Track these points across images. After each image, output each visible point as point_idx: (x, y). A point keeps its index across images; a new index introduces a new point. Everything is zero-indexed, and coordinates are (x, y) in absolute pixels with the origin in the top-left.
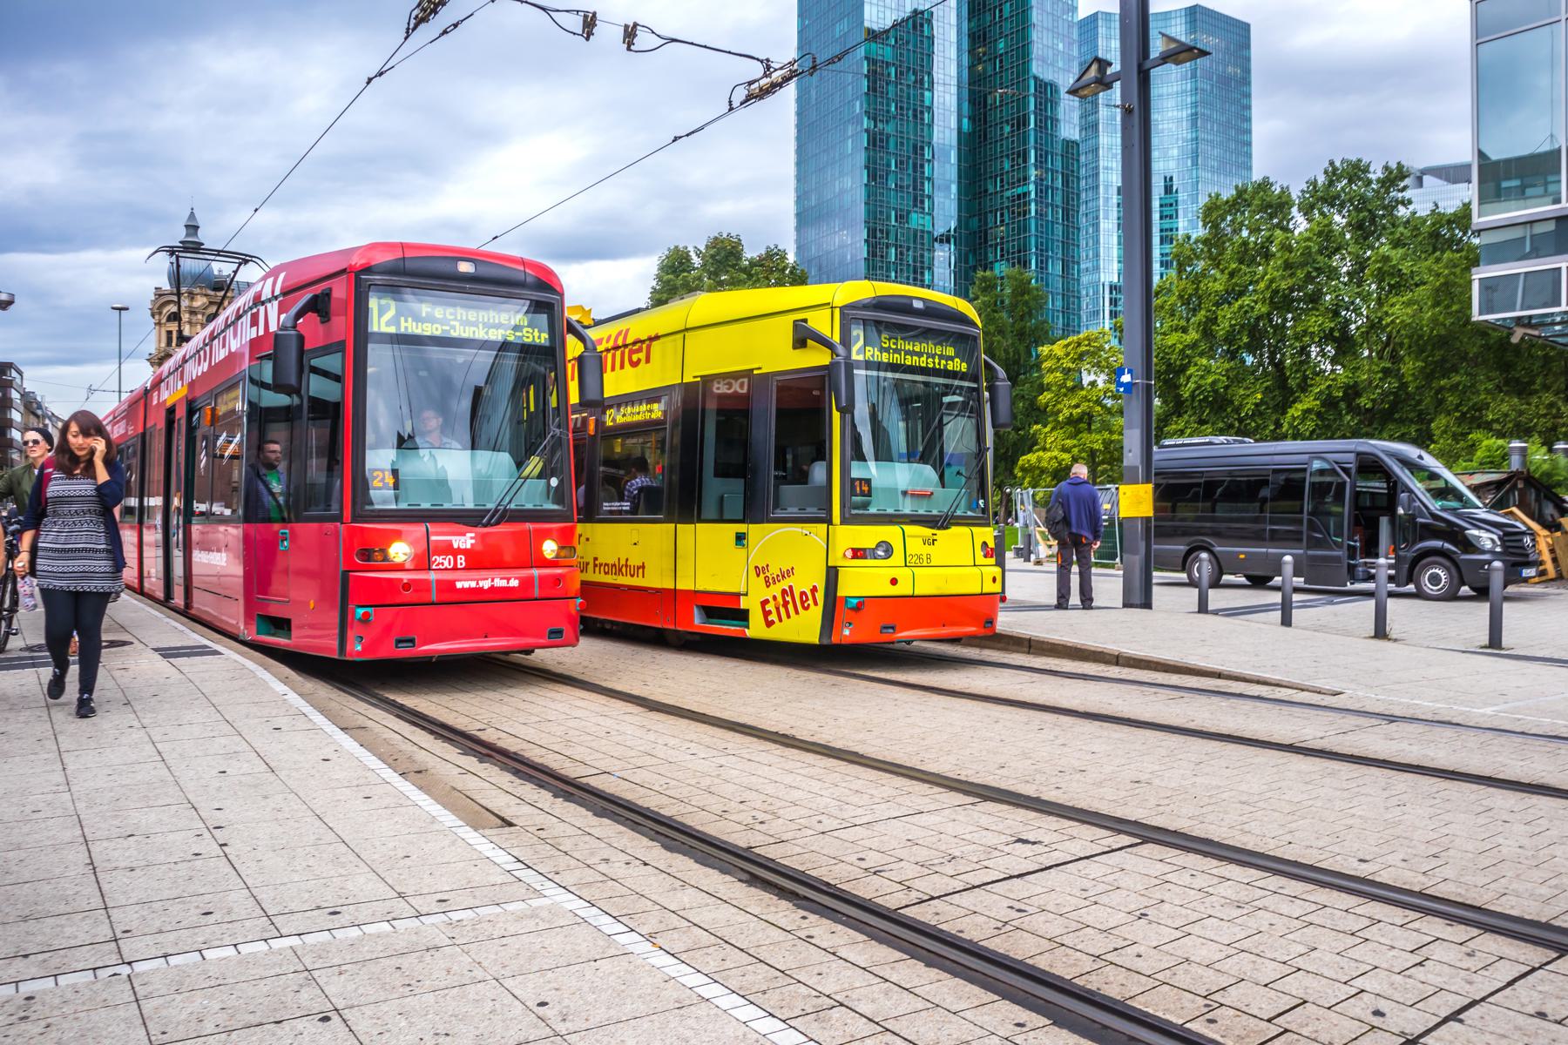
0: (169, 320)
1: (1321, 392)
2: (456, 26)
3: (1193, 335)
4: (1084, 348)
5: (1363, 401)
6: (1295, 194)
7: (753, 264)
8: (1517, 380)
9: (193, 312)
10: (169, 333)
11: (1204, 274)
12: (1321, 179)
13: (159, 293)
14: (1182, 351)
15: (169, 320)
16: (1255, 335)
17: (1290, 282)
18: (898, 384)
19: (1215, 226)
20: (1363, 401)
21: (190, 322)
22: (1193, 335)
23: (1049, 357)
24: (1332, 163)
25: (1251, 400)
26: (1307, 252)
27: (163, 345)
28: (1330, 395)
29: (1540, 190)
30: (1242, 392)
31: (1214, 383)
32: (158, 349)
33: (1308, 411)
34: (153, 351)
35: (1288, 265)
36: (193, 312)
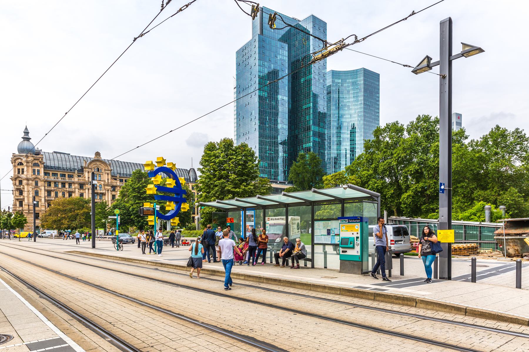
0: (18, 165)
1: (413, 189)
2: (187, 6)
3: (371, 172)
4: (337, 177)
5: (428, 192)
6: (405, 127)
7: (237, 148)
8: (482, 185)
9: (27, 162)
10: (19, 169)
11: (374, 152)
12: (415, 120)
13: (14, 155)
14: (367, 176)
15: (18, 165)
16: (390, 171)
17: (405, 154)
18: (322, 188)
19: (378, 137)
20: (428, 192)
21: (27, 166)
22: (371, 172)
23: (326, 180)
24: (419, 116)
25: (390, 192)
26: (411, 145)
27: (16, 173)
28: (416, 190)
29: (46, 195)
30: (386, 190)
31: (378, 186)
32: (15, 175)
33: (410, 196)
34: (13, 176)
35: (404, 149)
36: (27, 162)
